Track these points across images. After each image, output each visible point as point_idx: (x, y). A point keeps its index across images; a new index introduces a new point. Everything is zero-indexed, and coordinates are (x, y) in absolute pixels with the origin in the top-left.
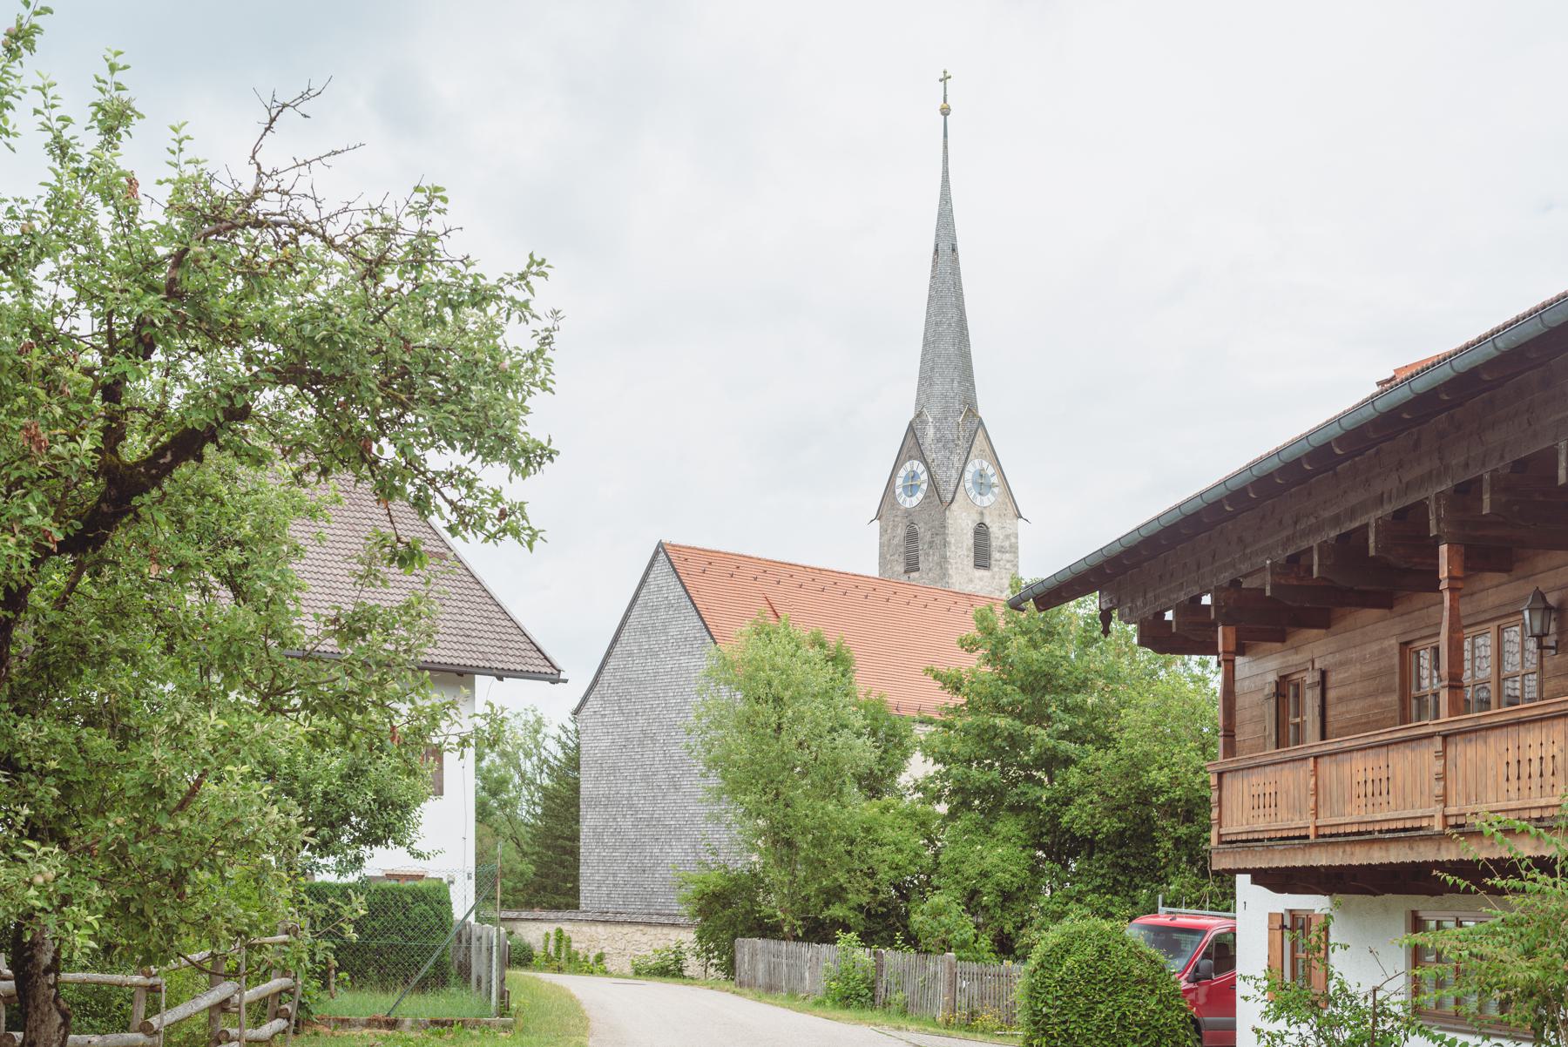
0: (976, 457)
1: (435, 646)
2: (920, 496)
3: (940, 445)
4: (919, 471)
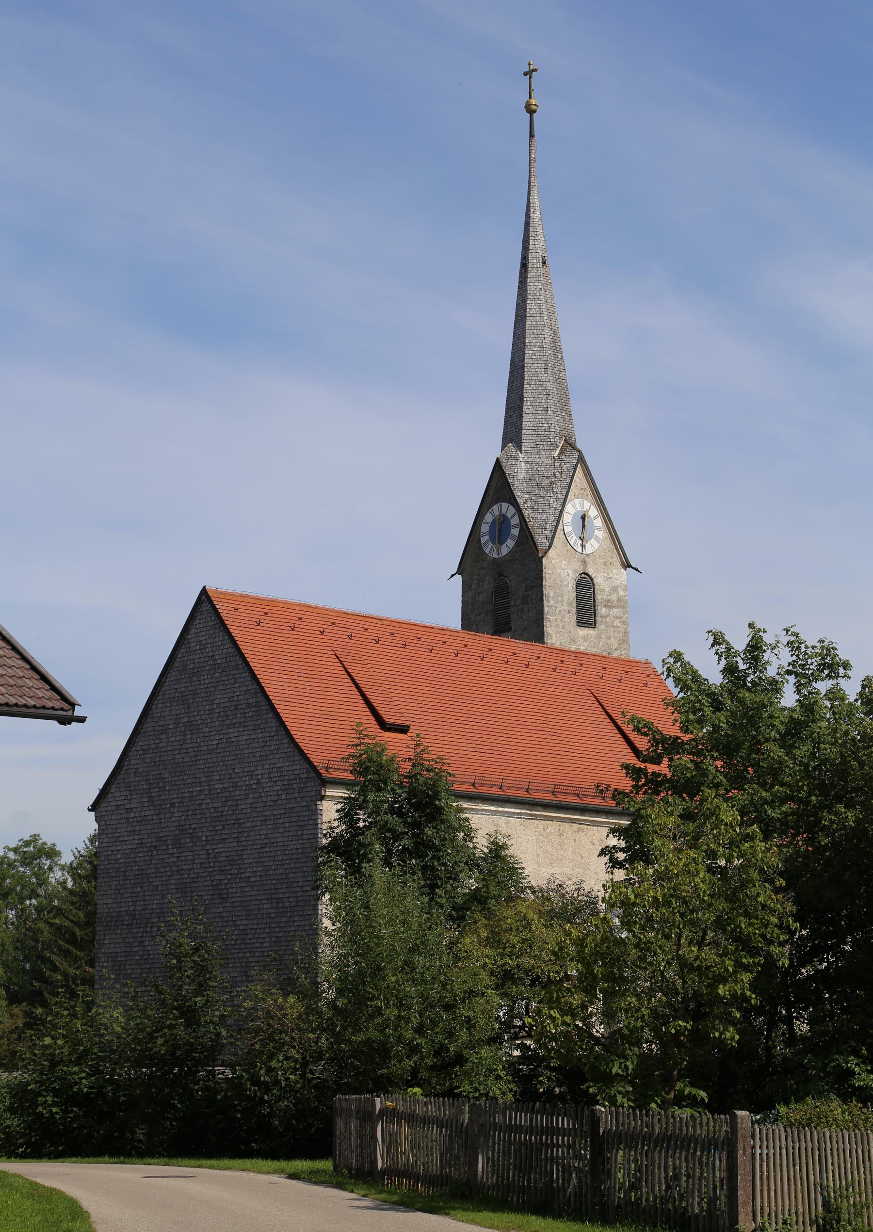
0: (575, 496)
1: (176, 689)
2: (510, 543)
3: (534, 483)
4: (509, 515)
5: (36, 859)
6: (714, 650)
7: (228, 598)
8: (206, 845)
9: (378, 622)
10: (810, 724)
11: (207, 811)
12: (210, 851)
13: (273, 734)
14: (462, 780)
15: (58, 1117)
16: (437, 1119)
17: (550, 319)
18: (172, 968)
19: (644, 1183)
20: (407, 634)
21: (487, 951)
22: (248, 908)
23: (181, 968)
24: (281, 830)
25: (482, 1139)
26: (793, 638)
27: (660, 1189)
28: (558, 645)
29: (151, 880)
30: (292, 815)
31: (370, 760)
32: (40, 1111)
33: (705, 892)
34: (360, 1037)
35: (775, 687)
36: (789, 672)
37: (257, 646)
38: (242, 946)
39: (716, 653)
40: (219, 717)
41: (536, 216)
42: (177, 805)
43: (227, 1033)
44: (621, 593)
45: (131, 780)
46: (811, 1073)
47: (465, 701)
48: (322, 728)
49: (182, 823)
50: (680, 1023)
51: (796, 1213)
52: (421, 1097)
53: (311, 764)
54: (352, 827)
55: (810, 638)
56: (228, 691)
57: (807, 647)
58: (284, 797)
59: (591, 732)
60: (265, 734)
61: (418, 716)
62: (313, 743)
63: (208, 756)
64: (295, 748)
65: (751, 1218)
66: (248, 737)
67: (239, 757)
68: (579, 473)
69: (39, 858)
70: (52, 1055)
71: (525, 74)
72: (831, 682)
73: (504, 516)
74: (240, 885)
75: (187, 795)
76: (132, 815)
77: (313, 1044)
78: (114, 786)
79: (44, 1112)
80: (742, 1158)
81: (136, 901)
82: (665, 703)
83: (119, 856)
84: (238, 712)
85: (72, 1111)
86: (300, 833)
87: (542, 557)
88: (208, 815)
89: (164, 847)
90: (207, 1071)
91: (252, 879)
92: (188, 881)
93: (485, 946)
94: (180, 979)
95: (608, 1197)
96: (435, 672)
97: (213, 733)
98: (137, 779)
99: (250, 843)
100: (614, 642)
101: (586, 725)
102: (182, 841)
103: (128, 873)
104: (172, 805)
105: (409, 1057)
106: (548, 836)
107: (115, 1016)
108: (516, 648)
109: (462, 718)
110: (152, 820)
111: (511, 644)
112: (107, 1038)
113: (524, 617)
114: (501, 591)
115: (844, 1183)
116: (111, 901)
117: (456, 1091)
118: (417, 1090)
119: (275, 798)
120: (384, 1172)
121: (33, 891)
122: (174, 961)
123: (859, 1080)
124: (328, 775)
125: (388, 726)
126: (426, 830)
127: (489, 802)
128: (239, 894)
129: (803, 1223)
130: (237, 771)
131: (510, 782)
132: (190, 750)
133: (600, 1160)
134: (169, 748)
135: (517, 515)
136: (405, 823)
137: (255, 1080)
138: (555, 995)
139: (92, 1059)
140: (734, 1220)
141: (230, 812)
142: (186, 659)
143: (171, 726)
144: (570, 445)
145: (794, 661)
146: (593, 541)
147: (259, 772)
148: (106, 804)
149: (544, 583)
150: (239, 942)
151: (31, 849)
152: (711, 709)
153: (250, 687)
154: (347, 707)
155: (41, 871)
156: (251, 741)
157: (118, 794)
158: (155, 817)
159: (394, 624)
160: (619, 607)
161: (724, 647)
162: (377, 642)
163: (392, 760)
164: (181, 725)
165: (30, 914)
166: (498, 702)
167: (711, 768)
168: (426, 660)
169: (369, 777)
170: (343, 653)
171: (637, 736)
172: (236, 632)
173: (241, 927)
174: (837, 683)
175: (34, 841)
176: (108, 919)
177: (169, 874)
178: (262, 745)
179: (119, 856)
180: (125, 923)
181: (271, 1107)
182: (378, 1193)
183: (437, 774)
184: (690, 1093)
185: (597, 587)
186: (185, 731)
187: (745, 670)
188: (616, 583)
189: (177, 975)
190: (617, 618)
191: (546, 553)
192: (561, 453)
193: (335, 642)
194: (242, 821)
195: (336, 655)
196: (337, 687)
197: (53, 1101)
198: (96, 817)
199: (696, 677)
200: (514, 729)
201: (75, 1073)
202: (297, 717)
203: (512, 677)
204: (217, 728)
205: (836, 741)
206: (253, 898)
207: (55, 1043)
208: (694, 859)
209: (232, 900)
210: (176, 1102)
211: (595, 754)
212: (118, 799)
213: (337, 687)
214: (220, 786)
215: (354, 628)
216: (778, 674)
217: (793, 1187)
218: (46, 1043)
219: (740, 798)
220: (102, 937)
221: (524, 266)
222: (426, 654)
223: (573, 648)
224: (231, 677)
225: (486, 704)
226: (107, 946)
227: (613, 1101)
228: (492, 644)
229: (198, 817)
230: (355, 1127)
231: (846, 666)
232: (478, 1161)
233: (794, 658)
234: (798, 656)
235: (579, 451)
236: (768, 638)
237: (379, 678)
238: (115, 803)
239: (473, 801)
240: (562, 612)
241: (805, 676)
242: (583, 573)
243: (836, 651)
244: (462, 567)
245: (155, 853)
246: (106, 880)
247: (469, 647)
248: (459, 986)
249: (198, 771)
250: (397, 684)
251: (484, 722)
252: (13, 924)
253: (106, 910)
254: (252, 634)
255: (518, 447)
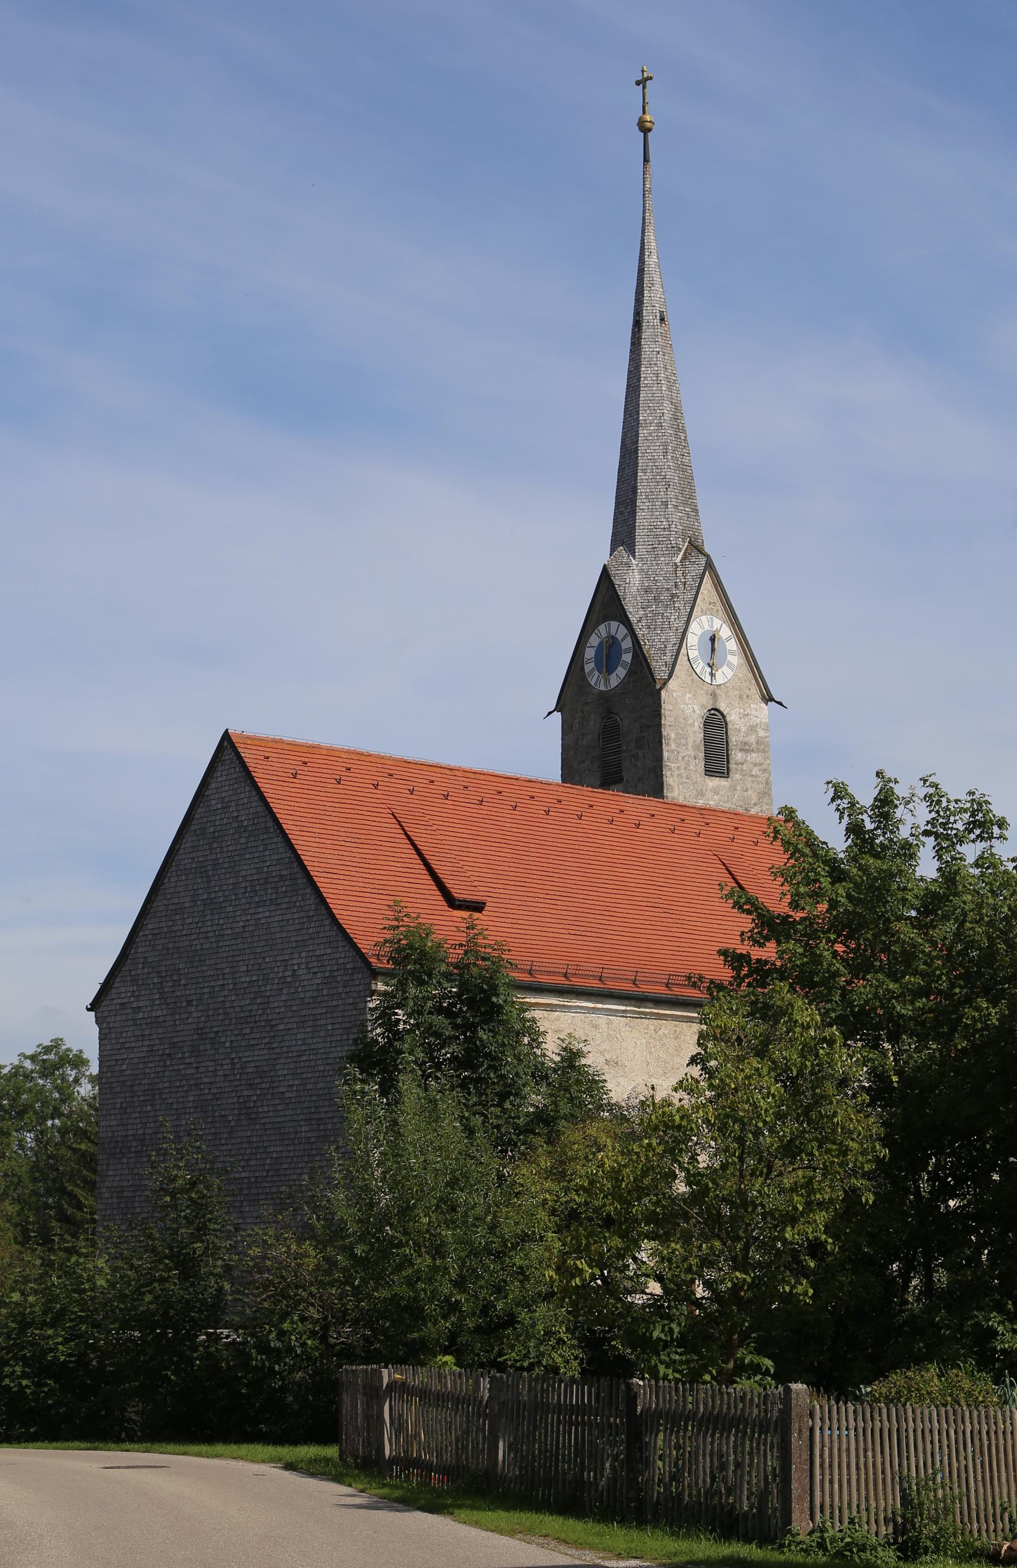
0: (703, 613)
2: (621, 672)
3: (651, 597)
4: (619, 637)
5: (58, 1069)
6: (834, 806)
7: (257, 743)
8: (230, 1053)
9: (448, 772)
10: (951, 898)
11: (232, 1010)
12: (236, 1061)
13: (311, 913)
14: (551, 969)
15: (28, 1391)
16: (453, 1395)
17: (670, 389)
18: (164, 1207)
19: (686, 1474)
20: (484, 787)
21: (548, 1184)
22: (282, 1131)
23: (176, 1206)
24: (323, 1033)
25: (504, 1420)
26: (931, 790)
27: (704, 1481)
28: (681, 800)
29: (164, 1096)
30: (335, 1015)
31: (410, 946)
32: (6, 1385)
33: (766, 1111)
34: (384, 1293)
35: (908, 851)
36: (927, 833)
37: (292, 804)
38: (276, 1179)
39: (837, 810)
40: (245, 893)
41: (652, 260)
42: (195, 1003)
43: (231, 1287)
44: (762, 733)
45: (139, 972)
46: (944, 1334)
47: (557, 870)
48: (373, 906)
49: (201, 1025)
50: (738, 1274)
51: (867, 1510)
52: (455, 1368)
53: (357, 950)
54: (389, 1030)
55: (955, 791)
56: (256, 860)
57: (948, 801)
58: (325, 992)
59: (718, 909)
60: (301, 915)
61: (497, 890)
62: (362, 924)
63: (233, 942)
64: (338, 931)
65: (808, 1517)
66: (281, 918)
67: (270, 942)
68: (707, 582)
69: (62, 1066)
70: (23, 1314)
71: (638, 83)
72: (983, 845)
73: (613, 638)
74: (272, 1103)
75: (206, 990)
76: (140, 1015)
77: (336, 1301)
78: (117, 980)
79: (12, 1385)
80: (797, 1443)
81: (146, 1123)
82: (772, 872)
83: (124, 1067)
84: (268, 886)
85: (46, 1385)
86: (345, 1037)
87: (661, 689)
88: (233, 1015)
89: (180, 1056)
90: (207, 1334)
91: (287, 1095)
92: (209, 1097)
93: (546, 1179)
94: (174, 1220)
95: (646, 1492)
96: (520, 835)
97: (238, 913)
98: (146, 971)
99: (285, 1049)
100: (752, 795)
101: (711, 899)
102: (202, 1048)
103: (136, 1088)
104: (189, 1003)
105: (445, 1317)
106: (660, 1040)
107: (100, 1266)
108: (624, 804)
109: (552, 893)
110: (165, 1021)
111: (618, 798)
112: (89, 1293)
113: (639, 764)
114: (610, 732)
115: (930, 1471)
116: (115, 1123)
117: (499, 1360)
118: (449, 1358)
119: (315, 994)
120: (394, 1461)
121: (56, 1109)
122: (168, 1199)
123: (1003, 1342)
124: (379, 965)
125: (457, 903)
126: (481, 1033)
127: (586, 997)
128: (271, 1114)
129: (876, 1521)
130: (267, 960)
131: (612, 971)
132: (210, 935)
133: (637, 1446)
134: (185, 932)
135: (629, 637)
136: (455, 1027)
137: (264, 1347)
138: (584, 1242)
139: (71, 1320)
140: (788, 1520)
141: (260, 1012)
142: (205, 820)
143: (187, 905)
144: (696, 548)
145: (934, 819)
146: (725, 669)
147: (295, 962)
148: (109, 1002)
149: (663, 722)
150: (271, 1173)
151: (52, 1057)
152: (828, 879)
153: (283, 856)
154: (405, 880)
155: (65, 1084)
156: (285, 923)
157: (123, 990)
158: (168, 1018)
159: (468, 775)
160: (758, 751)
161: (846, 801)
162: (446, 797)
163: (440, 946)
164: (199, 903)
165: (53, 1136)
166: (599, 872)
167: (826, 953)
168: (509, 820)
169: (409, 967)
170: (402, 812)
171: (738, 915)
172: (267, 786)
173: (274, 1155)
174: (991, 846)
175: (55, 1047)
176: (112, 1145)
177: (186, 1088)
178: (298, 927)
179: (124, 1067)
180: (133, 1149)
181: (283, 1379)
182: (380, 1488)
183: (493, 963)
184: (752, 1361)
185: (730, 726)
186: (204, 911)
187: (872, 830)
188: (755, 721)
189: (172, 1216)
190: (756, 765)
191: (665, 684)
192: (684, 558)
193: (392, 798)
194: (274, 1023)
195: (393, 815)
196: (393, 854)
197: (23, 1372)
198: (96, 1018)
199: (811, 841)
200: (619, 906)
201: (49, 1337)
202: (341, 892)
203: (618, 840)
204: (244, 907)
205: (982, 919)
206: (288, 1119)
207: (26, 1300)
208: (757, 1070)
209: (263, 1121)
210: (169, 1373)
211: (722, 935)
212: (123, 995)
213: (393, 854)
214: (248, 979)
215: (417, 780)
216: (912, 835)
217: (863, 1476)
218: (13, 1300)
219: (863, 991)
220: (105, 1167)
221: (638, 324)
222: (508, 812)
223: (700, 803)
224: (260, 843)
225: (584, 874)
226: (111, 1179)
227: (654, 1374)
228: (592, 799)
229: (221, 1017)
230: (362, 1405)
231: (1002, 824)
232: (498, 1448)
233: (934, 815)
234: (938, 812)
235: (707, 556)
236: (900, 791)
237: (447, 842)
238: (119, 1001)
239: (565, 995)
240: (686, 758)
241: (947, 837)
242: (712, 709)
243: (990, 806)
244: (562, 702)
245: (168, 1063)
246: (109, 1096)
247: (563, 802)
248: (508, 1229)
249: (220, 960)
250: (471, 850)
251: (581, 896)
252: (31, 1148)
253: (110, 1134)
254: (287, 789)
255: (630, 551)
